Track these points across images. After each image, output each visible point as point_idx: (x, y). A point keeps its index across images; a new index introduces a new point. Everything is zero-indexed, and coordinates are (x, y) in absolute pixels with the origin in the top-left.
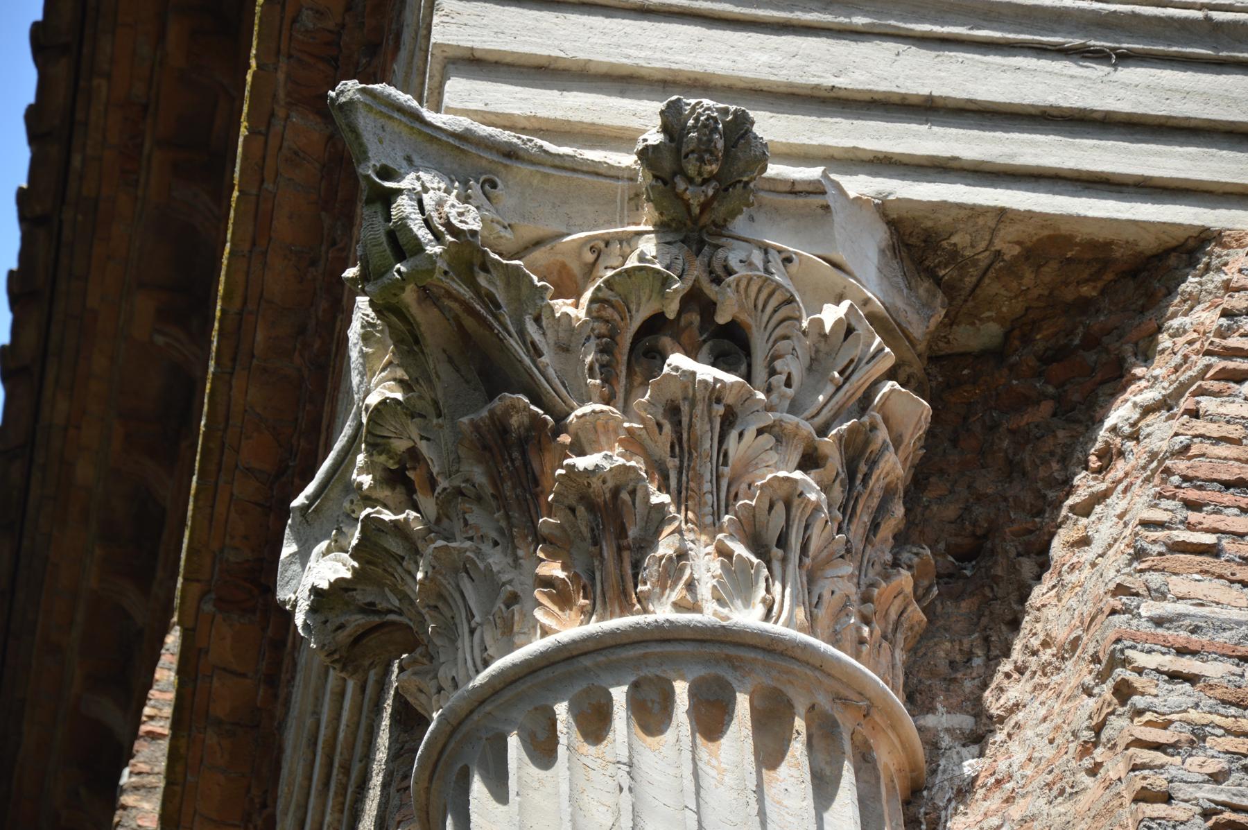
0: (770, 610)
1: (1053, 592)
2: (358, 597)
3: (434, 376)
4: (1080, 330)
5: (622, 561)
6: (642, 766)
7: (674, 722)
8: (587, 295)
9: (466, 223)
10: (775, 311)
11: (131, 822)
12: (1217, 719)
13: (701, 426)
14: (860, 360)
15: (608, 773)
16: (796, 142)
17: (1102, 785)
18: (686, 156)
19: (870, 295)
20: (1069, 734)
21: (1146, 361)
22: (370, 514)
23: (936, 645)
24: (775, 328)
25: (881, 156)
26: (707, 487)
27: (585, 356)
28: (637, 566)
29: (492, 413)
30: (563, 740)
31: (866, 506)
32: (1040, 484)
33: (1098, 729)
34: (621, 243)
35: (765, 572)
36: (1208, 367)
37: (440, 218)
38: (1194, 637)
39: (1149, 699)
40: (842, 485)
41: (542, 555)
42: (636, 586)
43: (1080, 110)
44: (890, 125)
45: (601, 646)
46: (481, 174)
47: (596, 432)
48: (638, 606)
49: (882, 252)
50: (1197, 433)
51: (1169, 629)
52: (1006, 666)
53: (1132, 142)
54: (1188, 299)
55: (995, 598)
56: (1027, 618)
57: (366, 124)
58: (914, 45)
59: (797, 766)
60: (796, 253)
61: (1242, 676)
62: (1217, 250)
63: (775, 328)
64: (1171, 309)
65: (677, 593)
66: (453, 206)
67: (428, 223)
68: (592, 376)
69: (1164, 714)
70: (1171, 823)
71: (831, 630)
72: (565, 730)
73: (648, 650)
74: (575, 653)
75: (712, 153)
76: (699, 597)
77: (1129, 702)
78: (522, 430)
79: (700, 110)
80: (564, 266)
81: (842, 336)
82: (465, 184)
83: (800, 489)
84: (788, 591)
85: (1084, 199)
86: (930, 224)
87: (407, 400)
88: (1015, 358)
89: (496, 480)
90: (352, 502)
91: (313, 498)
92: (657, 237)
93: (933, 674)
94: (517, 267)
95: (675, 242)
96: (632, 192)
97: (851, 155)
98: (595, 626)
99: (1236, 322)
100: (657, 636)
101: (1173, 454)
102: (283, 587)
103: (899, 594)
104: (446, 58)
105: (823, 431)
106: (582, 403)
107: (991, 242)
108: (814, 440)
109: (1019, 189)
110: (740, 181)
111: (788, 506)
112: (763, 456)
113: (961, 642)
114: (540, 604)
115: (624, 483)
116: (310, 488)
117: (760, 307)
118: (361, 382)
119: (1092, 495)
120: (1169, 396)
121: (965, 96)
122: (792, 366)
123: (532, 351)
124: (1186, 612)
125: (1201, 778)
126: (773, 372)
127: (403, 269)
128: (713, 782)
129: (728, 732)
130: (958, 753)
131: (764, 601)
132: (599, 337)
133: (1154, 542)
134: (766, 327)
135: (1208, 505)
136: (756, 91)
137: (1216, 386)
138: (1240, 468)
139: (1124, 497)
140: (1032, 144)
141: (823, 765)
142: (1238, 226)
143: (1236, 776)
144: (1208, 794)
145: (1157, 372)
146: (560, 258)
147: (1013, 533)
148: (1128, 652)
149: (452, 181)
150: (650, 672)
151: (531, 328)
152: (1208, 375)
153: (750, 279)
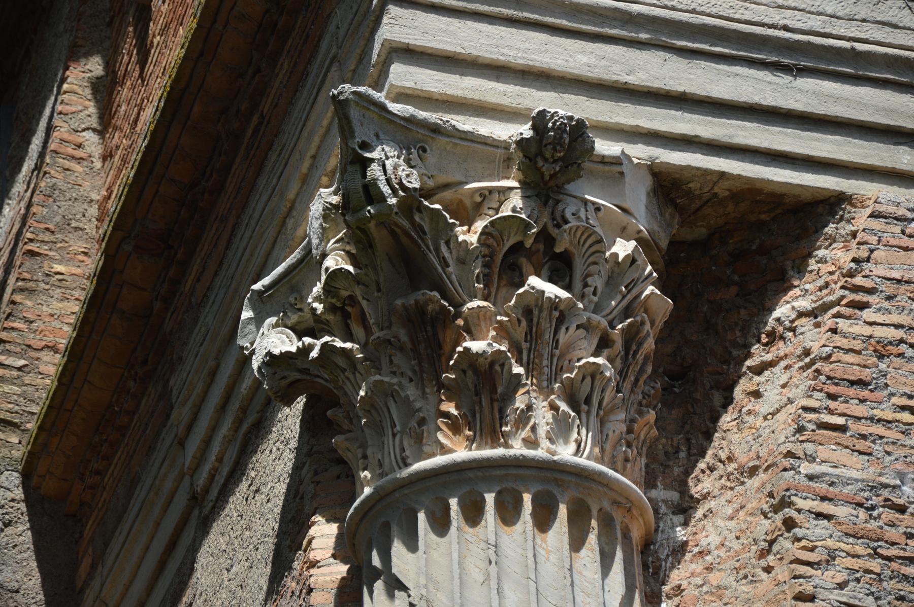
0: (579, 446)
2: (299, 364)
4: (757, 241)
5: (493, 409)
7: (522, 519)
8: (479, 225)
9: (411, 183)
12: (842, 546)
13: (545, 324)
14: (638, 279)
15: (481, 547)
16: (602, 120)
17: (773, 583)
18: (546, 146)
19: (642, 228)
20: (751, 540)
21: (799, 273)
22: (328, 342)
24: (589, 257)
25: (652, 132)
26: (545, 362)
27: (475, 269)
29: (417, 302)
30: (454, 523)
33: (771, 543)
35: (578, 422)
36: (843, 297)
37: (396, 178)
38: (831, 489)
40: (621, 359)
41: (443, 398)
42: (501, 427)
43: (773, 107)
44: (658, 110)
47: (479, 318)
48: (502, 440)
49: (648, 194)
50: (836, 345)
51: (816, 482)
52: (702, 465)
53: (802, 130)
55: (695, 413)
56: (716, 435)
58: (675, 54)
59: (592, 550)
60: (603, 205)
61: (857, 517)
62: (848, 207)
63: (589, 257)
64: (818, 243)
65: (525, 433)
66: (404, 170)
67: (388, 181)
69: (812, 541)
72: (456, 517)
74: (463, 468)
75: (561, 146)
76: (538, 436)
77: (792, 531)
79: (557, 118)
80: (461, 201)
82: (408, 149)
83: (602, 369)
85: (772, 168)
86: (677, 176)
90: (296, 299)
91: (268, 288)
95: (532, 196)
96: (506, 156)
97: (634, 130)
99: (860, 267)
102: (242, 337)
104: (391, 48)
107: (712, 188)
108: (607, 330)
110: (576, 163)
111: (593, 377)
112: (579, 342)
113: (672, 440)
114: (441, 430)
115: (498, 359)
116: (266, 281)
117: (582, 243)
118: (320, 244)
119: (762, 362)
120: (816, 308)
121: (705, 94)
122: (597, 282)
123: (443, 263)
127: (372, 211)
128: (543, 559)
129: (554, 527)
130: (671, 519)
131: (576, 441)
132: (484, 256)
133: (810, 421)
135: (841, 397)
136: (578, 81)
137: (849, 311)
138: (860, 372)
139: (785, 373)
142: (862, 192)
143: (852, 584)
145: (807, 286)
146: (459, 196)
148: (793, 498)
149: (401, 149)
150: (509, 485)
151: (444, 249)
152: (843, 302)
153: (578, 227)
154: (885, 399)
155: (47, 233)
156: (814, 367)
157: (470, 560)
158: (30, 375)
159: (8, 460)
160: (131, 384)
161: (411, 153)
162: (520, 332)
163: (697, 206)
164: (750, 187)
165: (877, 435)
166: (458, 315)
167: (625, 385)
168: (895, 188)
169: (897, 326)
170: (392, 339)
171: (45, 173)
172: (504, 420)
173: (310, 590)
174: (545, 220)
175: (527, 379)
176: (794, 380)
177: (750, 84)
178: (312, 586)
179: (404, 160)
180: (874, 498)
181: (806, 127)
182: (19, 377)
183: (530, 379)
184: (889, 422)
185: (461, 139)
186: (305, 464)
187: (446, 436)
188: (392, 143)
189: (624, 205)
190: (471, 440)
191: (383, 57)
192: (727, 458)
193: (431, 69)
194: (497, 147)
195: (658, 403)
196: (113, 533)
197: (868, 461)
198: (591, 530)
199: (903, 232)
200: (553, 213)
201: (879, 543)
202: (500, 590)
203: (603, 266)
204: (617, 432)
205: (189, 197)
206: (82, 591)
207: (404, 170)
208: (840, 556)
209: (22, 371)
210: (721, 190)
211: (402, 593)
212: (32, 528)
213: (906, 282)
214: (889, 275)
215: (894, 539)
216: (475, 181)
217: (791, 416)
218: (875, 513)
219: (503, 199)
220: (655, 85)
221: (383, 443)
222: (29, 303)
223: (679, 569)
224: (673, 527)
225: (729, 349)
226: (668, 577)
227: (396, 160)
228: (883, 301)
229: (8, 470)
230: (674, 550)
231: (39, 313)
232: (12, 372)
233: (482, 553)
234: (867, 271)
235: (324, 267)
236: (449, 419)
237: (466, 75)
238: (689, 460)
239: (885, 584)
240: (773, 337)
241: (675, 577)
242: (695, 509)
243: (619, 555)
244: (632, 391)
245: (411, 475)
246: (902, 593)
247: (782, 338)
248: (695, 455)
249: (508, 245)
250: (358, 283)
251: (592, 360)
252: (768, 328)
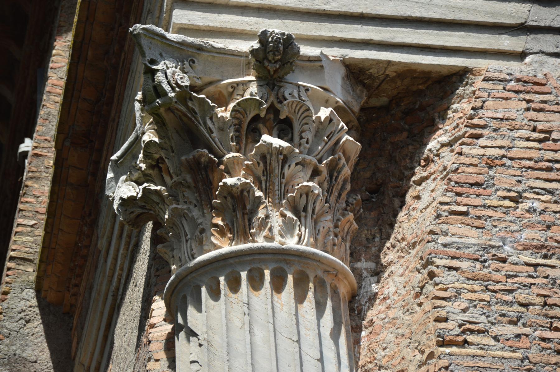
0: (300, 238)
1: (406, 217)
3: (171, 138)
4: (418, 103)
6: (253, 303)
7: (265, 286)
8: (231, 106)
11: (30, 193)
12: (465, 286)
13: (274, 164)
14: (335, 131)
15: (240, 305)
17: (423, 312)
18: (269, 52)
19: (339, 100)
20: (411, 287)
23: (362, 232)
24: (302, 120)
25: (343, 39)
26: (276, 188)
27: (230, 133)
28: (250, 220)
29: (194, 157)
30: (223, 292)
31: (336, 189)
32: (402, 168)
33: (422, 288)
34: (243, 85)
35: (299, 223)
36: (466, 132)
37: (174, 81)
38: (458, 251)
39: (441, 279)
40: (327, 182)
41: (214, 215)
42: (250, 230)
43: (420, 17)
46: (189, 57)
47: (234, 164)
48: (251, 238)
49: (343, 78)
50: (461, 162)
51: (449, 248)
52: (388, 245)
53: (439, 31)
54: (459, 97)
55: (384, 213)
56: (396, 225)
57: (144, 42)
59: (310, 302)
60: (310, 87)
61: (475, 267)
62: (471, 76)
63: (302, 120)
64: (453, 100)
65: (265, 233)
66: (179, 75)
67: (169, 83)
68: (232, 142)
69: (446, 285)
70: (447, 330)
71: (323, 242)
72: (223, 288)
73: (255, 258)
74: (227, 257)
75: (278, 52)
76: (274, 233)
78: (205, 163)
79: (274, 35)
80: (220, 92)
81: (328, 123)
82: (183, 62)
83: (312, 189)
84: (307, 230)
86: (361, 66)
87: (160, 143)
89: (195, 181)
91: (120, 158)
92: (257, 83)
93: (360, 244)
95: (264, 85)
96: (247, 62)
97: (331, 39)
101: (452, 171)
103: (348, 221)
105: (320, 161)
107: (385, 71)
108: (317, 165)
109: (396, 52)
110: (289, 62)
111: (307, 195)
112: (298, 174)
113: (371, 231)
114: (213, 235)
115: (245, 189)
116: (119, 153)
117: (297, 112)
118: (141, 127)
119: (421, 177)
120: (451, 141)
121: (375, 13)
122: (309, 135)
124: (455, 241)
125: (459, 311)
126: (301, 138)
127: (159, 102)
128: (279, 309)
129: (285, 290)
130: (369, 280)
131: (298, 235)
133: (444, 211)
134: (299, 120)
135: (464, 194)
138: (477, 177)
139: (434, 182)
141: (320, 298)
142: (479, 66)
144: (461, 317)
145: (447, 128)
146: (219, 89)
147: (391, 187)
148: (434, 259)
149: (178, 62)
151: (209, 122)
152: (466, 135)
153: (293, 102)
154: (493, 193)
155: (46, 142)
156: (447, 178)
157: (233, 314)
158: (39, 229)
159: (27, 282)
160: (85, 228)
161: (184, 64)
162: (259, 170)
163: (378, 84)
164: (408, 68)
165: (488, 216)
166: (221, 163)
167: (331, 198)
168: (501, 62)
169: (500, 147)
170: (183, 182)
171: (44, 105)
172: (251, 226)
174: (272, 99)
175: (266, 199)
176: (438, 186)
177: (405, 4)
178: (150, 339)
179: (180, 69)
180: (486, 255)
181: (442, 28)
182: (32, 231)
183: (267, 199)
184: (496, 207)
185: (217, 53)
186: (152, 265)
188: (171, 59)
189: (325, 86)
190: (232, 240)
191: (169, 6)
192: (401, 239)
193: (199, 11)
194: (241, 56)
195: (360, 209)
196: (85, 321)
197: (482, 232)
198: (310, 289)
199: (504, 89)
200: (277, 95)
201: (489, 283)
202: (251, 331)
203: (312, 125)
204: (326, 228)
205: (96, 108)
206: (74, 359)
207: (179, 75)
208: (464, 293)
209: (34, 227)
210: (390, 71)
211: (195, 338)
212: (43, 323)
213: (506, 119)
214: (495, 116)
215: (498, 279)
216: (228, 79)
217: (434, 209)
218: (487, 264)
220: (343, 10)
221: (181, 246)
222: (36, 186)
223: (372, 309)
224: (371, 284)
225: (403, 171)
226: (366, 315)
227: (174, 69)
228: (492, 132)
229: (27, 289)
230: (370, 298)
231: (43, 191)
232: (27, 229)
233: (241, 309)
234: (481, 115)
235: (142, 140)
236: (218, 228)
238: (381, 242)
239: (493, 307)
240: (428, 161)
241: (370, 315)
242: (383, 272)
243: (329, 304)
244: (337, 201)
245: (195, 264)
246: (503, 312)
247: (433, 161)
248: (384, 239)
250: (162, 149)
251: (305, 184)
252: (425, 156)
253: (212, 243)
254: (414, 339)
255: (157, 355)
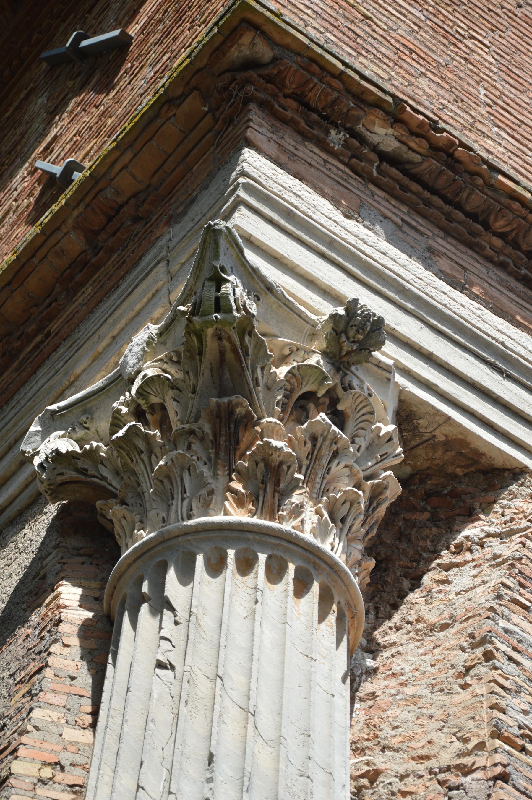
2: (79, 463)
4: (450, 487)
7: (284, 581)
10: (363, 415)
14: (389, 455)
18: (351, 326)
25: (406, 369)
26: (318, 480)
27: (278, 395)
29: (230, 402)
32: (419, 548)
38: (519, 644)
41: (234, 478)
42: (278, 511)
45: (259, 531)
52: (388, 624)
55: (384, 592)
64: (503, 495)
65: (296, 522)
74: (245, 529)
75: (363, 330)
77: (491, 662)
86: (415, 409)
88: (413, 487)
90: (87, 418)
91: (61, 409)
94: (263, 341)
96: (312, 332)
98: (255, 520)
100: (287, 538)
106: (269, 416)
107: (435, 430)
110: (368, 349)
112: (343, 478)
116: (62, 404)
117: (358, 410)
120: (503, 533)
121: (445, 360)
125: (519, 710)
127: (219, 317)
129: (306, 597)
140: (466, 394)
147: (399, 565)
148: (493, 639)
150: (279, 553)
151: (259, 371)
173: (60, 621)
185: (285, 304)
187: (231, 505)
194: (307, 322)
198: (331, 612)
211: (170, 613)
219: (307, 357)
237: (286, 274)
240: (459, 549)
249: (305, 389)
253: (225, 507)
254: (450, 723)
255: (69, 639)
